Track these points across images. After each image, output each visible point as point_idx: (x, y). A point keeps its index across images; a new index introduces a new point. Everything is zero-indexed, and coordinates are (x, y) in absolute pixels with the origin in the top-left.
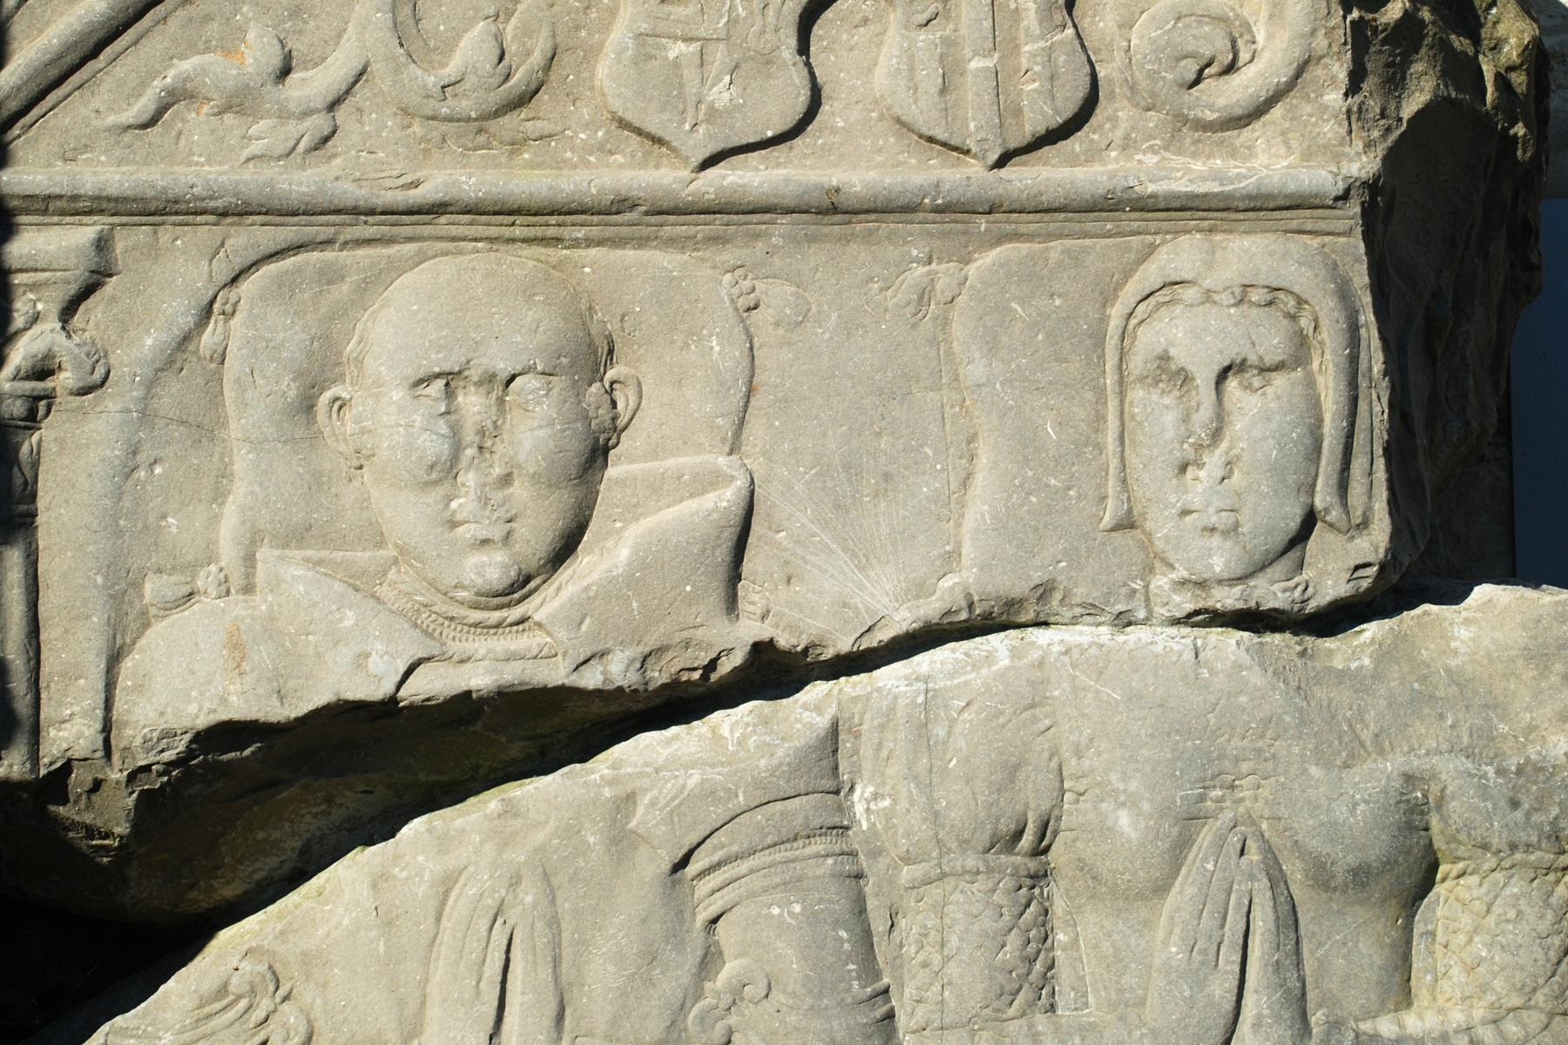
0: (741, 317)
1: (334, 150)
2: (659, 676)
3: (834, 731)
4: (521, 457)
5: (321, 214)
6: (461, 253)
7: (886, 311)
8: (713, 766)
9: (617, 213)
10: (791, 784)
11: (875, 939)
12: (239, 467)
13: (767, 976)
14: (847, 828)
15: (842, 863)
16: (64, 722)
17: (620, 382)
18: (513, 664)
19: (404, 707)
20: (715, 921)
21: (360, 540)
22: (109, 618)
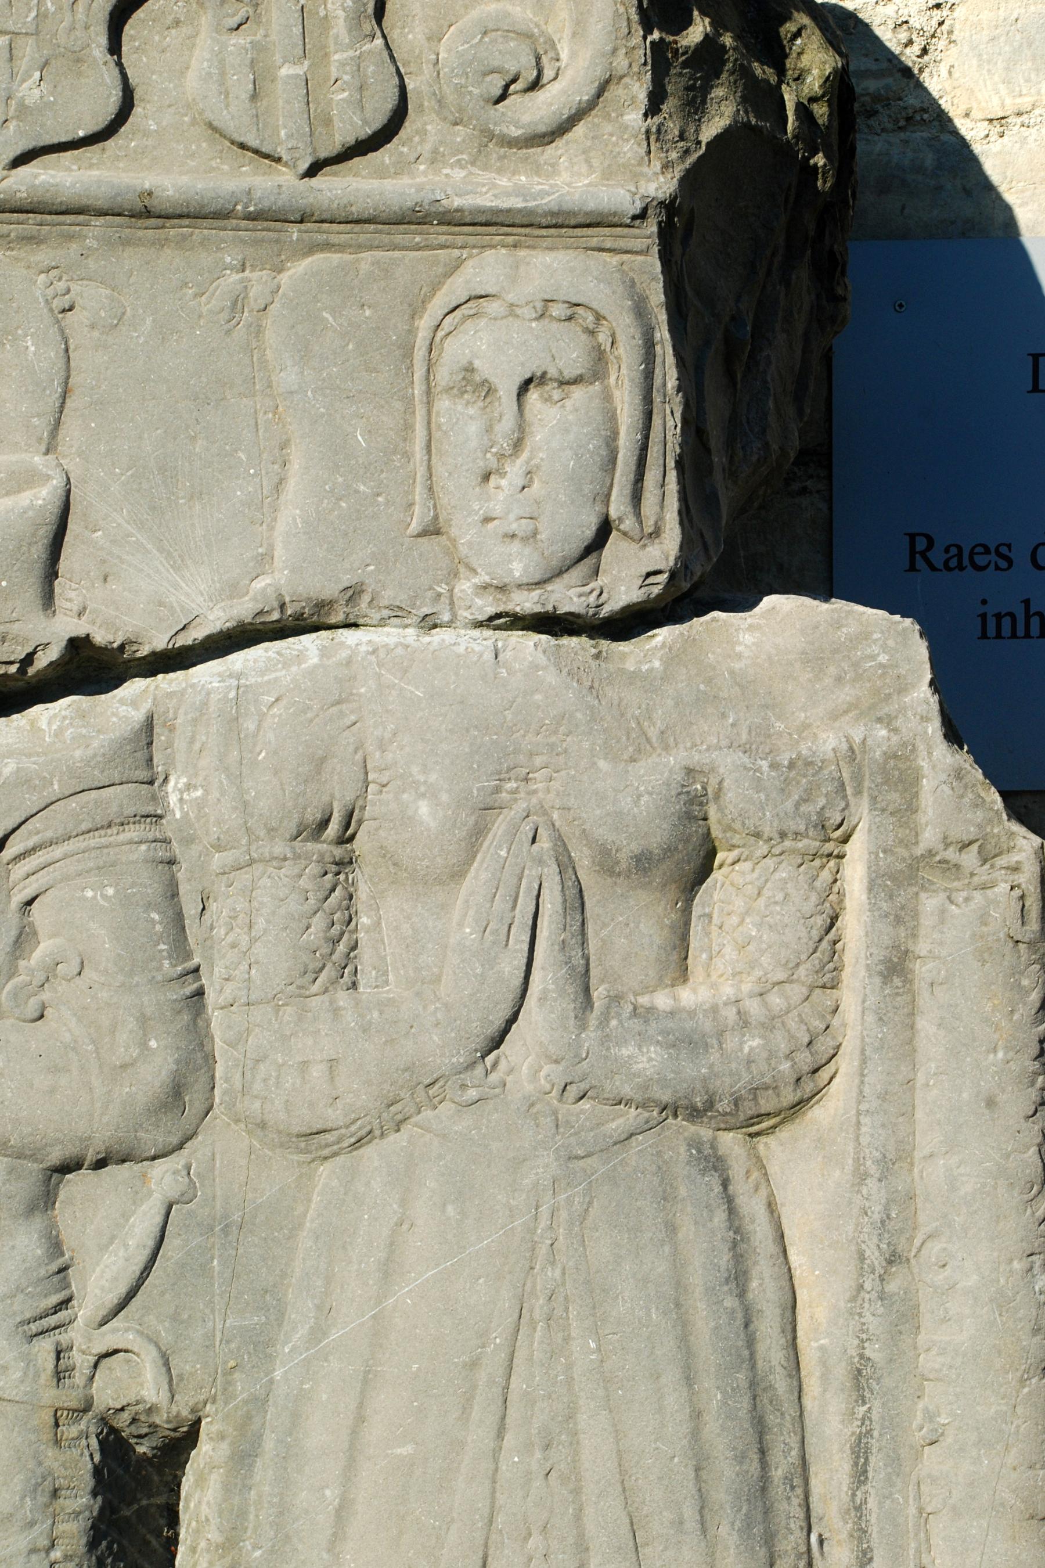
3: (149, 725)
7: (200, 316)
8: (29, 755)
10: (105, 774)
11: (187, 922)
13: (80, 955)
14: (161, 817)
15: (155, 850)
20: (30, 903)
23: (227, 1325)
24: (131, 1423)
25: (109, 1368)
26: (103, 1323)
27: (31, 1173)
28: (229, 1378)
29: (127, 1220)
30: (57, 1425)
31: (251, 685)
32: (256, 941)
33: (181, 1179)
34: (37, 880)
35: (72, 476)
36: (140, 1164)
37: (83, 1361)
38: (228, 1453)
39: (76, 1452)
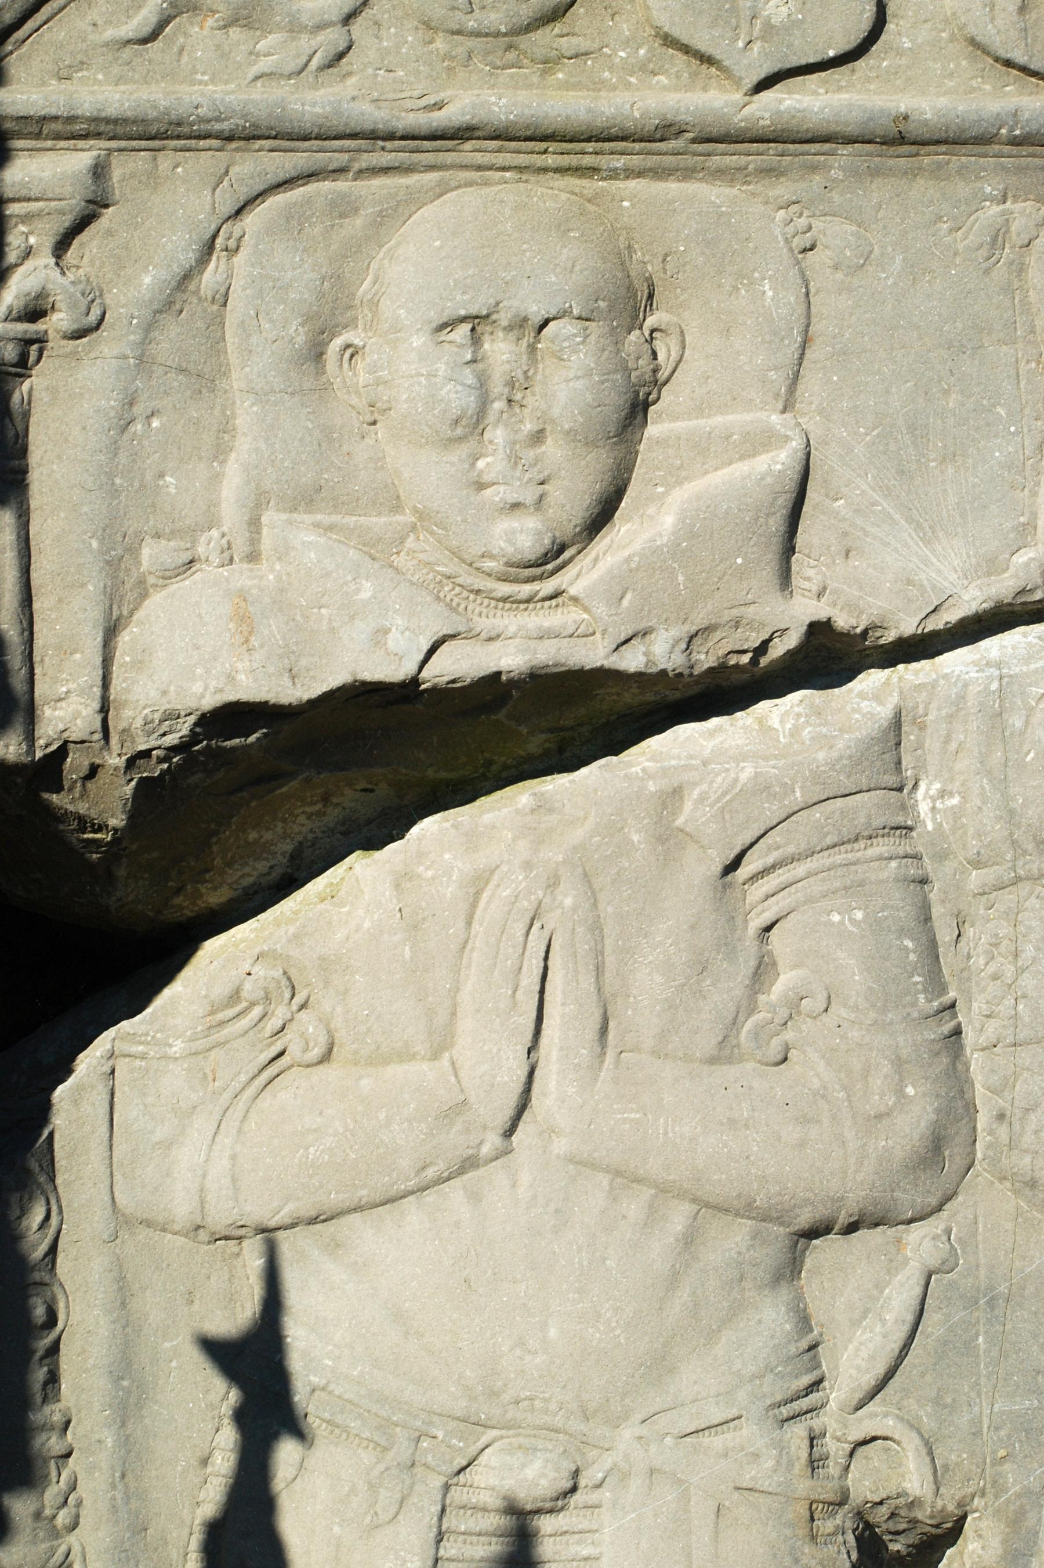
0: (796, 259)
1: (349, 68)
2: (705, 659)
3: (897, 723)
4: (556, 412)
5: (335, 138)
6: (487, 183)
7: (955, 254)
8: (766, 759)
9: (661, 140)
10: (852, 779)
11: (941, 950)
12: (241, 421)
13: (827, 989)
14: (910, 829)
15: (907, 866)
16: (60, 700)
17: (661, 330)
18: (547, 642)
19: (426, 690)
20: (768, 929)
21: (374, 503)
22: (105, 587)
23: (996, 1410)
24: (889, 1518)
25: (866, 1458)
26: (858, 1408)
27: (777, 1237)
28: (999, 1468)
29: (882, 1292)
30: (812, 1519)
31: (1016, 675)
32: (1023, 971)
33: (941, 1246)
34: (778, 903)
35: (811, 437)
36: (894, 1229)
37: (837, 1450)
38: (1000, 1551)
39: (832, 1549)
